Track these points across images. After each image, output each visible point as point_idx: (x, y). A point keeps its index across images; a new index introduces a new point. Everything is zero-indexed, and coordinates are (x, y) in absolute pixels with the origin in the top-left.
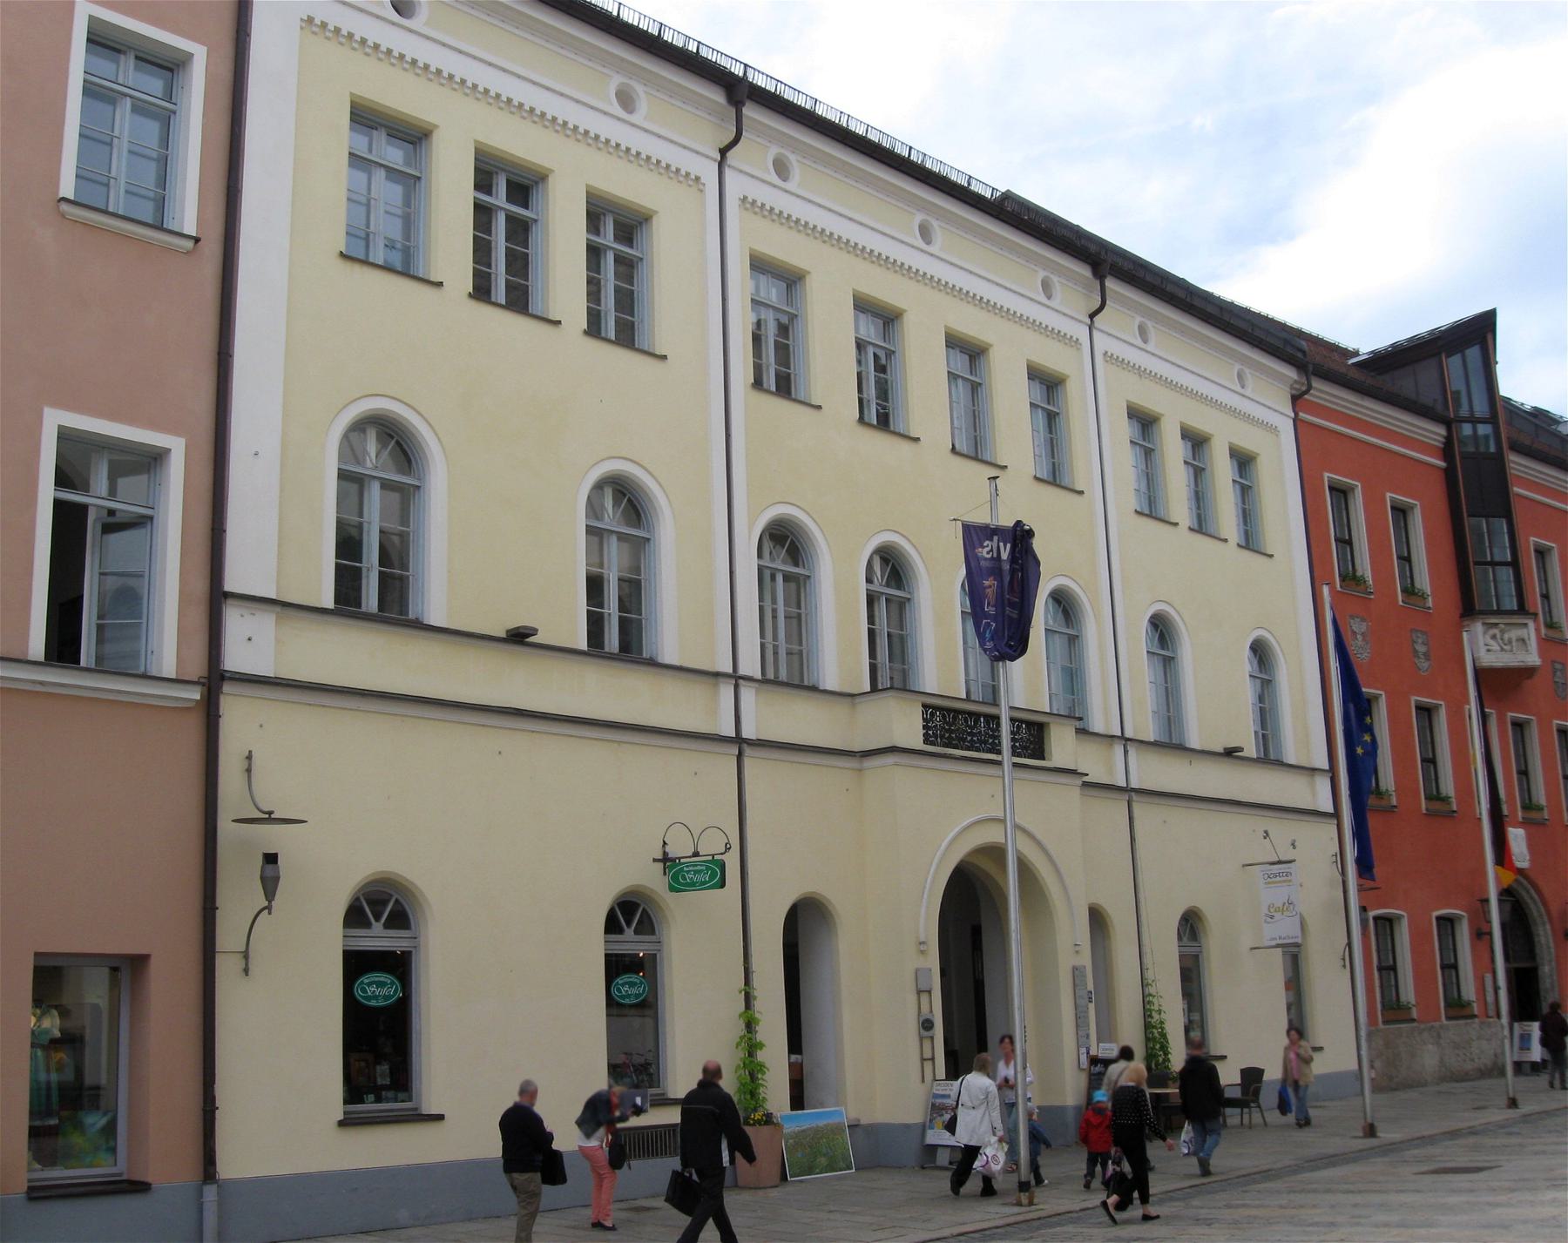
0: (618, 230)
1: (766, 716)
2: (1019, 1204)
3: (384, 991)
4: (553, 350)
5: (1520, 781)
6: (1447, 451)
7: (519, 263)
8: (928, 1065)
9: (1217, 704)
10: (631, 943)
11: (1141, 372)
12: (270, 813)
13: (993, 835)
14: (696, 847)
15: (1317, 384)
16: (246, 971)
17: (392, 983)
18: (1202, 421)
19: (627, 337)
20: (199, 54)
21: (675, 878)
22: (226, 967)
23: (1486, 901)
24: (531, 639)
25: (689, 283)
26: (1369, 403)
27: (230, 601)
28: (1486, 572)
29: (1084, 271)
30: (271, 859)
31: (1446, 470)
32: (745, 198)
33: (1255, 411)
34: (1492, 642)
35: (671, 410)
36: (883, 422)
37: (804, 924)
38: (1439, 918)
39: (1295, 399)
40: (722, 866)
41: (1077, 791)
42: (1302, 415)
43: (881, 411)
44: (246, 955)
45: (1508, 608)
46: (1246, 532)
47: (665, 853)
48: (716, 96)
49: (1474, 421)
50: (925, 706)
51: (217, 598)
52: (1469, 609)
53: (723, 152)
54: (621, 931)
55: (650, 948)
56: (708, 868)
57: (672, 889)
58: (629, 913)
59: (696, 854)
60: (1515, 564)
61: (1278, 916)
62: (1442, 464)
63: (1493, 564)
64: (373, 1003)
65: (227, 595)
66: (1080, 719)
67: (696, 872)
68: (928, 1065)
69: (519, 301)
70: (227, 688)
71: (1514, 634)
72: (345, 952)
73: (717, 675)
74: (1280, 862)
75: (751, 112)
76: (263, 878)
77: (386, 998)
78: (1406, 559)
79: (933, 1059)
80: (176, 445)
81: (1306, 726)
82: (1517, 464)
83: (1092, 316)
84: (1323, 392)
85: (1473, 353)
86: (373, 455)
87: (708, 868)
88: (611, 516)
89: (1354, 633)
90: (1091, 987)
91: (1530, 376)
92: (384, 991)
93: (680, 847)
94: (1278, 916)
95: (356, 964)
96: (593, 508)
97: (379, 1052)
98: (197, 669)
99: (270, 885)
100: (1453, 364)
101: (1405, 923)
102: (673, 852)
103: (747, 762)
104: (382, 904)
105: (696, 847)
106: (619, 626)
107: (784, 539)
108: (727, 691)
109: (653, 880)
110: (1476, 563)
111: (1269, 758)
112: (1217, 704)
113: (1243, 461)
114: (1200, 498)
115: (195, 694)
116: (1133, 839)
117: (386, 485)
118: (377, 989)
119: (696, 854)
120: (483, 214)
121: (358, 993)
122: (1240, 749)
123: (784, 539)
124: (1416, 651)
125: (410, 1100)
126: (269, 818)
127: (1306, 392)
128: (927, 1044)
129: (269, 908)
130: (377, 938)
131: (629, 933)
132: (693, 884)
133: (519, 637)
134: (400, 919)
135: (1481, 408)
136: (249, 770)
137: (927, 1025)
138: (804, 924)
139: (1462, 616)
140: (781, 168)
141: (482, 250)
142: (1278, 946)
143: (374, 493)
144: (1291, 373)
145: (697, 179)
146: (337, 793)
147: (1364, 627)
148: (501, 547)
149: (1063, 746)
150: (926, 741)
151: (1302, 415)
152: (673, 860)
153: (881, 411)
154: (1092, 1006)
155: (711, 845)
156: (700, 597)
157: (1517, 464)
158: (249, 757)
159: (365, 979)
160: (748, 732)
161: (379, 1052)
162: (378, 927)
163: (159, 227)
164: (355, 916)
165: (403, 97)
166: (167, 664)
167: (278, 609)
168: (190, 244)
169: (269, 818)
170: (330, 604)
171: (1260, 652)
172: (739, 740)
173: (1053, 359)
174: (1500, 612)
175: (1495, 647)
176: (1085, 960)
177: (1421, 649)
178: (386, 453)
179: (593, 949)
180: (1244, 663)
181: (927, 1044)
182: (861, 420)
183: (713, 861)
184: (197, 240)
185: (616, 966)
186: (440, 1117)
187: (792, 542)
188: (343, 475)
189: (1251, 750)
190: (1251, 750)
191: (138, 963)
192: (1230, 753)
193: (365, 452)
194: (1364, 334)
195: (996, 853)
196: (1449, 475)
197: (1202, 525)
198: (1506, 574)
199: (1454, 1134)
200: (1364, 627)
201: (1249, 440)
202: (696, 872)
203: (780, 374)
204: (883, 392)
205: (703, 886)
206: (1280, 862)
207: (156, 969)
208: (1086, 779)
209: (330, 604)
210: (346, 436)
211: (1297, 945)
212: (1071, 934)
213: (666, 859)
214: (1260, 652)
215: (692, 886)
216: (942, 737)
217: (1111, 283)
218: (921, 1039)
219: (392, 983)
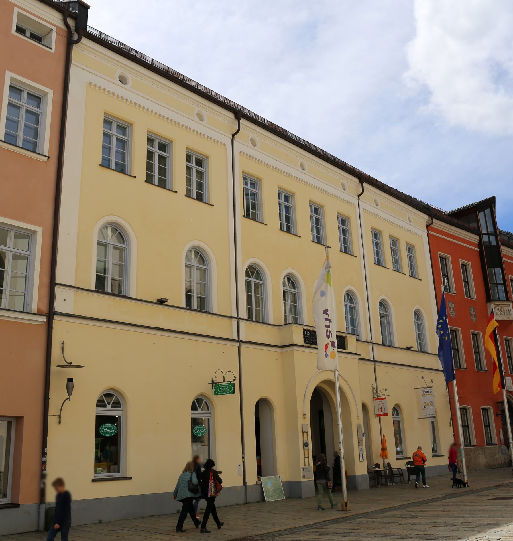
0: (197, 163)
1: (249, 331)
2: (320, 509)
3: (111, 431)
4: (175, 201)
5: (509, 360)
6: (480, 244)
7: (162, 171)
8: (307, 459)
9: (403, 332)
10: (200, 414)
11: (376, 216)
12: (71, 363)
13: (330, 376)
14: (224, 378)
15: (435, 220)
16: (60, 422)
17: (114, 428)
18: (396, 234)
19: (199, 198)
20: (51, 93)
21: (216, 390)
22: (52, 420)
23: (503, 402)
24: (166, 303)
25: (220, 183)
26: (453, 228)
27: (57, 286)
28: (494, 287)
29: (356, 180)
30: (70, 380)
31: (479, 251)
32: (241, 152)
33: (414, 230)
34: (497, 311)
35: (214, 223)
36: (288, 230)
37: (262, 406)
38: (482, 409)
39: (428, 226)
40: (234, 385)
41: (357, 361)
42: (430, 232)
43: (288, 226)
44: (60, 417)
45: (502, 299)
46: (412, 272)
47: (213, 381)
48: (231, 115)
49: (488, 234)
50: (304, 330)
51: (53, 285)
52: (489, 299)
53: (233, 135)
54: (197, 409)
55: (208, 416)
56: (229, 386)
57: (215, 394)
58: (197, 404)
59: (224, 381)
60: (504, 283)
61: (427, 407)
62: (478, 250)
63: (497, 284)
64: (106, 435)
65: (56, 284)
66: (358, 335)
67: (224, 388)
68: (307, 459)
69: (162, 184)
70: (56, 317)
71: (506, 308)
72: (97, 416)
73: (231, 317)
74: (428, 387)
75: (243, 121)
76: (67, 387)
77: (111, 433)
78: (467, 282)
79: (308, 457)
80: (40, 231)
81: (433, 342)
82: (504, 250)
83: (359, 196)
84: (438, 224)
85: (488, 211)
86: (110, 236)
87: (229, 386)
88: (194, 261)
89: (450, 307)
90: (363, 432)
91: (507, 220)
92: (111, 431)
93: (219, 380)
94: (427, 407)
95: (101, 420)
96: (188, 258)
97: (108, 451)
98: (45, 308)
99: (70, 389)
100: (481, 215)
101: (471, 410)
102: (216, 380)
103: (242, 349)
104: (110, 398)
105: (224, 378)
106: (196, 302)
107: (253, 271)
108: (235, 322)
109: (209, 391)
110: (491, 284)
111: (422, 350)
112: (403, 332)
113: (410, 249)
114: (396, 261)
115: (44, 319)
116: (351, 390)
117: (115, 248)
118: (108, 430)
119: (224, 381)
120: (150, 155)
121: (101, 431)
122: (412, 347)
123: (253, 271)
124: (471, 314)
125: (118, 471)
126: (70, 365)
127: (432, 224)
128: (306, 451)
129: (69, 399)
130: (109, 411)
131: (200, 410)
132: (223, 392)
133: (161, 302)
134: (117, 404)
135: (491, 230)
136: (63, 348)
137: (306, 445)
138: (262, 406)
139: (487, 302)
140: (253, 143)
141: (150, 167)
142: (427, 418)
143: (110, 249)
144: (426, 217)
145: (225, 144)
146: (97, 353)
147: (453, 305)
148: (156, 270)
149: (351, 343)
150: (305, 342)
151: (430, 232)
152: (216, 384)
153: (288, 226)
154: (364, 438)
155: (229, 378)
156: (225, 291)
157: (504, 250)
158: (63, 343)
159: (104, 426)
160: (242, 338)
161: (108, 451)
162: (109, 407)
163: (34, 152)
164: (101, 403)
165: (123, 113)
166: (34, 308)
167: (75, 289)
168: (46, 158)
169: (70, 365)
170: (94, 289)
171: (417, 315)
172: (239, 341)
173: (346, 211)
174: (499, 300)
175: (499, 313)
176: (361, 421)
177: (473, 313)
178: (114, 236)
179: (188, 414)
180: (413, 319)
181: (306, 451)
182: (281, 229)
183: (231, 384)
184: (49, 158)
185: (195, 422)
186: (131, 478)
187: (257, 271)
188: (100, 244)
189: (416, 348)
190: (416, 348)
191: (19, 419)
192: (409, 348)
193: (107, 235)
194: (448, 205)
195: (331, 383)
196: (481, 253)
197: (397, 269)
198: (501, 287)
199: (498, 486)
200: (453, 305)
201: (412, 241)
202: (224, 388)
203: (252, 211)
204: (288, 219)
205: (227, 393)
206: (428, 387)
207: (25, 420)
208: (360, 357)
209: (94, 289)
210: (101, 230)
211: (434, 417)
212: (356, 411)
213: (213, 383)
214: (417, 315)
215: (223, 393)
216: (310, 341)
217: (365, 184)
218: (304, 449)
219: (114, 428)
